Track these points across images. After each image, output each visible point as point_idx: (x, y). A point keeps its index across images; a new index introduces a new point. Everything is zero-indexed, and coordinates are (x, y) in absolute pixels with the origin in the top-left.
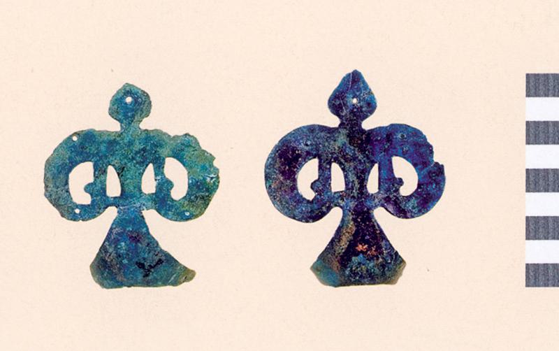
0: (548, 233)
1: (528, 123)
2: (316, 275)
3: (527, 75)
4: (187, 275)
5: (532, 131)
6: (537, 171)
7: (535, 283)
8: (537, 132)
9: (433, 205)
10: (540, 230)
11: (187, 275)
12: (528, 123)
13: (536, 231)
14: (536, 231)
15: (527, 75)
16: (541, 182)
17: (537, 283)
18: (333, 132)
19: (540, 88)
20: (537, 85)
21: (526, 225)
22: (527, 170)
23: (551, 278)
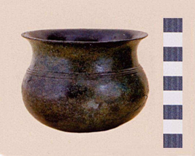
0: (176, 86)
1: (164, 77)
2: (135, 116)
3: (164, 19)
4: (23, 35)
5: (167, 53)
6: (169, 48)
7: (169, 59)
8: (169, 112)
9: (142, 109)
10: (171, 114)
11: (23, 35)
12: (164, 77)
13: (169, 56)
14: (169, 56)
15: (164, 19)
16: (172, 56)
17: (170, 59)
18: (96, 79)
19: (171, 85)
20: (170, 54)
21: (164, 27)
22: (164, 48)
23: (178, 85)
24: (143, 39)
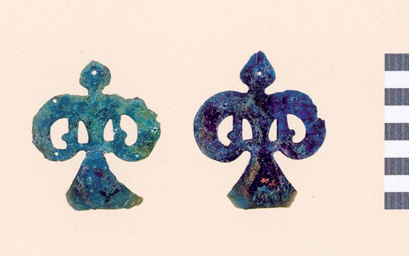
0: (401, 170)
1: (386, 90)
2: (231, 200)
3: (386, 55)
5: (389, 95)
6: (393, 125)
7: (391, 206)
8: (393, 97)
9: (317, 149)
10: (395, 168)
12: (386, 90)
13: (392, 169)
14: (392, 169)
15: (386, 55)
16: (396, 132)
17: (393, 206)
20: (393, 62)
21: (385, 164)
22: (386, 124)
23: (403, 203)
24: (281, 153)
